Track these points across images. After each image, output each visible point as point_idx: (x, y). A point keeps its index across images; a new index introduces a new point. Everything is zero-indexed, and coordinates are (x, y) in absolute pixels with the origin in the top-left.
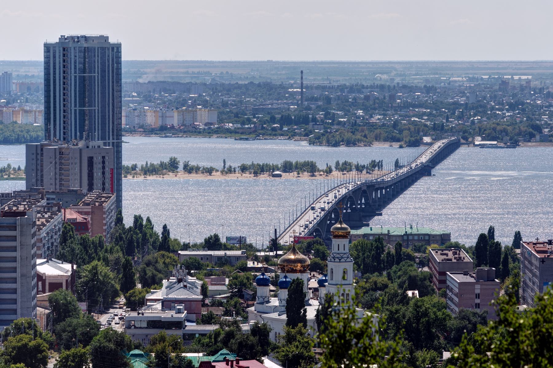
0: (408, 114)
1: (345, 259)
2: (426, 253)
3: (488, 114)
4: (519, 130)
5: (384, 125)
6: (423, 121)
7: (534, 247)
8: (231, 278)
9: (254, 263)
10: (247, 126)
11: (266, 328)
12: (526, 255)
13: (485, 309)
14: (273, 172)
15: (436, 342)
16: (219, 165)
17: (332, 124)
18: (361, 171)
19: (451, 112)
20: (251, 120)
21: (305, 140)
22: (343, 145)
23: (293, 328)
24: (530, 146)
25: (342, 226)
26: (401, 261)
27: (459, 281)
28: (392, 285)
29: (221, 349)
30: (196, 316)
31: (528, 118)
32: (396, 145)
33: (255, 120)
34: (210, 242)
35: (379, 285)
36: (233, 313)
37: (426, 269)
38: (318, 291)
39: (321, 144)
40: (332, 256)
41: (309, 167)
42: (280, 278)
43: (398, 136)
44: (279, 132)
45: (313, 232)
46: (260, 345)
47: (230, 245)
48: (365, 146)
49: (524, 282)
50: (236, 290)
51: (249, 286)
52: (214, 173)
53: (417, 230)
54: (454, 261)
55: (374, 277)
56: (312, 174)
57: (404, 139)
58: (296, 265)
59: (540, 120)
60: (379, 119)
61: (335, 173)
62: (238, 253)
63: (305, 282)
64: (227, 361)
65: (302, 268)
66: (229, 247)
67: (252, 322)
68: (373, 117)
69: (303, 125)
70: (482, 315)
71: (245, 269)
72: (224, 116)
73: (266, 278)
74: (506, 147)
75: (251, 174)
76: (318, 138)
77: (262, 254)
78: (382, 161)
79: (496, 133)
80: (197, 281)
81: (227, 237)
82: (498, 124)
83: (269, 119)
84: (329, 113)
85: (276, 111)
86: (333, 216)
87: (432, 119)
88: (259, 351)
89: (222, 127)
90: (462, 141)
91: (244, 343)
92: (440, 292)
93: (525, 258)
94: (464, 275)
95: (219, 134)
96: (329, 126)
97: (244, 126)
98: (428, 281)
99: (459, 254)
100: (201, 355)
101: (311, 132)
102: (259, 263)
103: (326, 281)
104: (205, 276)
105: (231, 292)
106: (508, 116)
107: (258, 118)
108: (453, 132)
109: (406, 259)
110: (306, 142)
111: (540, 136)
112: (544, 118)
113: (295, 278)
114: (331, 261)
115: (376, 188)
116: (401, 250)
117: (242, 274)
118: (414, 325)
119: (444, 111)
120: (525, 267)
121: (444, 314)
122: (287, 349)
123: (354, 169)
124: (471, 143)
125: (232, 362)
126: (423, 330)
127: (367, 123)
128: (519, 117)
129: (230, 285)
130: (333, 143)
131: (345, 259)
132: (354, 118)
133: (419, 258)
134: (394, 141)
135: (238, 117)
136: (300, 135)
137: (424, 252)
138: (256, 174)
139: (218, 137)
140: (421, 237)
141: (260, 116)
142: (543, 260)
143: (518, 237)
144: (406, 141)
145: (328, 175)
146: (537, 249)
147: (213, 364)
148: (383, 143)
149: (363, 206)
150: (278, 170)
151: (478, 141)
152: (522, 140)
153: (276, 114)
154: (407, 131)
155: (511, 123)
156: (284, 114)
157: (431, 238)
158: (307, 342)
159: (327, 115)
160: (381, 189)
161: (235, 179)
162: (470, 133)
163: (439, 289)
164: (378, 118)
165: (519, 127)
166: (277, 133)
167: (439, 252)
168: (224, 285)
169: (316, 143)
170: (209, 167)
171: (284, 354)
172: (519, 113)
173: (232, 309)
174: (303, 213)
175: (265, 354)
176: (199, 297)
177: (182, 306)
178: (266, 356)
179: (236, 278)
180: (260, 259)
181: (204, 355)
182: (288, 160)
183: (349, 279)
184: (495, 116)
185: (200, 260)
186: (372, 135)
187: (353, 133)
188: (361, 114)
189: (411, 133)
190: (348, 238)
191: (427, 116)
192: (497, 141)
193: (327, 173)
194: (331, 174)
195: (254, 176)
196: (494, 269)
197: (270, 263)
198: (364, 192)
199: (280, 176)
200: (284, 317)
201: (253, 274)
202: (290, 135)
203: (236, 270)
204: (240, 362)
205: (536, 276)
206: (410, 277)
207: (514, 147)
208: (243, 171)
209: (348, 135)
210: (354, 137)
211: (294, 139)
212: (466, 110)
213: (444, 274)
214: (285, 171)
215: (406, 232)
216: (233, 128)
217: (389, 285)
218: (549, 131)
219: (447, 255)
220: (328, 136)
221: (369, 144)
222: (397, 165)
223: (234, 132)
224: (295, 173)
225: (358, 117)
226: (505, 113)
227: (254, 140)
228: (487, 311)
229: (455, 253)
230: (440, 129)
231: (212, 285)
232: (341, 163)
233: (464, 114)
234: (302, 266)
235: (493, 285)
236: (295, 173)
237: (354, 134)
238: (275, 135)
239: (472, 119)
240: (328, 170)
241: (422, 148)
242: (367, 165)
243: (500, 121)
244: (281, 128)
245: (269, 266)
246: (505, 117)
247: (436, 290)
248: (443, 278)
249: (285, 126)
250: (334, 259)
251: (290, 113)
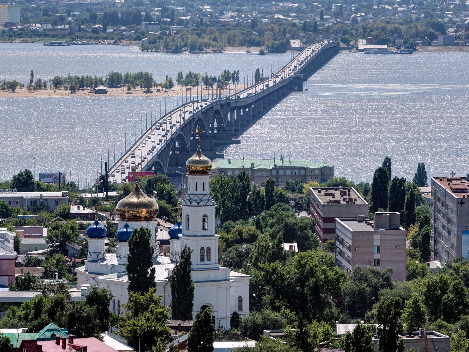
0: (270, 10)
1: (206, 202)
2: (302, 193)
3: (374, 9)
4: (416, 31)
5: (238, 25)
6: (290, 19)
7: (449, 184)
8: (50, 228)
9: (79, 207)
10: (59, 27)
11: (106, 295)
12: (439, 195)
13: (389, 267)
14: (96, 86)
15: (327, 310)
16: (24, 78)
17: (171, 23)
18: (211, 85)
19: (326, 6)
20: (65, 20)
21: (136, 45)
22: (186, 51)
23: (142, 294)
24: (430, 51)
25: (201, 158)
26: (273, 204)
27: (352, 231)
28: (262, 235)
29: (47, 324)
30: (9, 280)
31: (427, 14)
32: (255, 50)
33: (70, 19)
34: (21, 180)
35: (244, 236)
36: (55, 275)
37: (304, 214)
38: (169, 244)
39: (157, 50)
40: (188, 198)
41: (143, 80)
42: (119, 228)
43: (258, 38)
44: (102, 34)
45: (152, 165)
46: (98, 316)
47: (44, 184)
48: (215, 52)
49: (436, 230)
50: (57, 244)
51: (75, 238)
52: (18, 89)
53: (289, 163)
54: (343, 203)
55: (238, 226)
56: (146, 89)
57: (266, 43)
58: (140, 210)
59: (443, 17)
60: (232, 17)
61: (177, 88)
62: (58, 194)
63: (153, 233)
64: (58, 340)
65: (148, 215)
66: (44, 187)
67: (85, 286)
68: (223, 14)
69: (134, 25)
70: (384, 274)
71: (67, 216)
72: (29, 14)
73: (100, 229)
74: (399, 52)
75: (66, 90)
76: (154, 42)
77: (89, 195)
78: (238, 71)
79: (385, 34)
80: (8, 233)
81: (40, 174)
82: (388, 23)
83: (88, 18)
84: (167, 10)
85: (98, 6)
86: (177, 145)
87: (302, 16)
88: (97, 326)
89: (27, 28)
90: (342, 45)
91: (77, 315)
92: (325, 244)
93: (438, 199)
94: (359, 222)
95: (23, 37)
96: (167, 26)
97: (55, 27)
98: (309, 230)
99: (349, 195)
100: (20, 330)
101: (143, 35)
102: (86, 208)
103: (179, 231)
104: (16, 226)
105: (51, 247)
106: (401, 12)
107: (74, 16)
108: (330, 33)
109: (278, 201)
110: (137, 47)
111: (444, 38)
112: (448, 14)
113: (139, 228)
114: (186, 206)
115: (232, 107)
116: (273, 189)
117: (64, 222)
118: (297, 288)
119: (317, 6)
120: (437, 210)
121: (336, 273)
122: (135, 322)
123: (201, 82)
124: (353, 47)
125: (64, 340)
126: (310, 295)
127: (216, 22)
128: (416, 13)
129: (49, 238)
130: (174, 48)
131: (206, 202)
132: (199, 15)
133: (295, 200)
134: (253, 46)
135: (47, 15)
136: (129, 38)
137: (301, 191)
138: (73, 90)
139: (22, 42)
140: (294, 171)
141: (77, 13)
142: (461, 201)
143: (421, 170)
144: (268, 46)
145: (167, 90)
146: (454, 187)
147: (39, 343)
148: (238, 48)
149: (216, 132)
150: (102, 84)
151: (362, 44)
152: (420, 43)
153: (97, 11)
154: (269, 33)
155: (404, 21)
156: (107, 10)
157: (309, 174)
158: (162, 313)
159: (164, 11)
160: (239, 108)
161: (47, 96)
162: (352, 35)
163: (324, 241)
164: (231, 15)
165: (416, 26)
166: (99, 35)
167: (323, 192)
168: (41, 236)
169: (151, 49)
170: (12, 81)
171: (130, 328)
172: (414, 8)
173: (54, 269)
174: (138, 140)
175: (104, 329)
176: (12, 254)
178: (107, 332)
179: (57, 228)
180: (86, 202)
181: (24, 332)
182: (116, 71)
183: (209, 229)
184: (383, 12)
185: (8, 204)
186: (225, 37)
187: (199, 35)
188: (208, 10)
189: (274, 34)
190: (208, 174)
191: (296, 12)
192: (387, 44)
193: (167, 88)
194: (172, 89)
195: (71, 93)
196: (398, 213)
197: (100, 207)
198: (217, 112)
199: (105, 92)
200: (125, 279)
201: (78, 222)
202: (116, 38)
203: (55, 217)
204: (75, 340)
205: (453, 224)
206: (286, 224)
207: (410, 53)
208: (56, 87)
209: (192, 38)
210: (200, 40)
211: (122, 44)
212: (346, 4)
213: (332, 220)
214: (111, 86)
215: (275, 165)
216: (41, 30)
217: (259, 236)
218: (456, 32)
219: (333, 195)
220: (166, 40)
221: (219, 50)
222: (259, 78)
223: (42, 35)
224: (125, 88)
225: (205, 15)
226: (397, 8)
227: (70, 45)
228: (391, 270)
229: (343, 194)
230: (312, 29)
231: (25, 237)
232: (184, 76)
233: (344, 10)
234: (148, 212)
235: (396, 235)
236: (125, 88)
237: (200, 37)
238: (97, 38)
239: (353, 16)
240: (168, 84)
241: (289, 55)
242: (219, 77)
243: (390, 18)
244: (104, 30)
245: (99, 211)
246: (396, 14)
247: (320, 242)
248: (329, 226)
249: (110, 27)
250: (191, 203)
251: (116, 10)
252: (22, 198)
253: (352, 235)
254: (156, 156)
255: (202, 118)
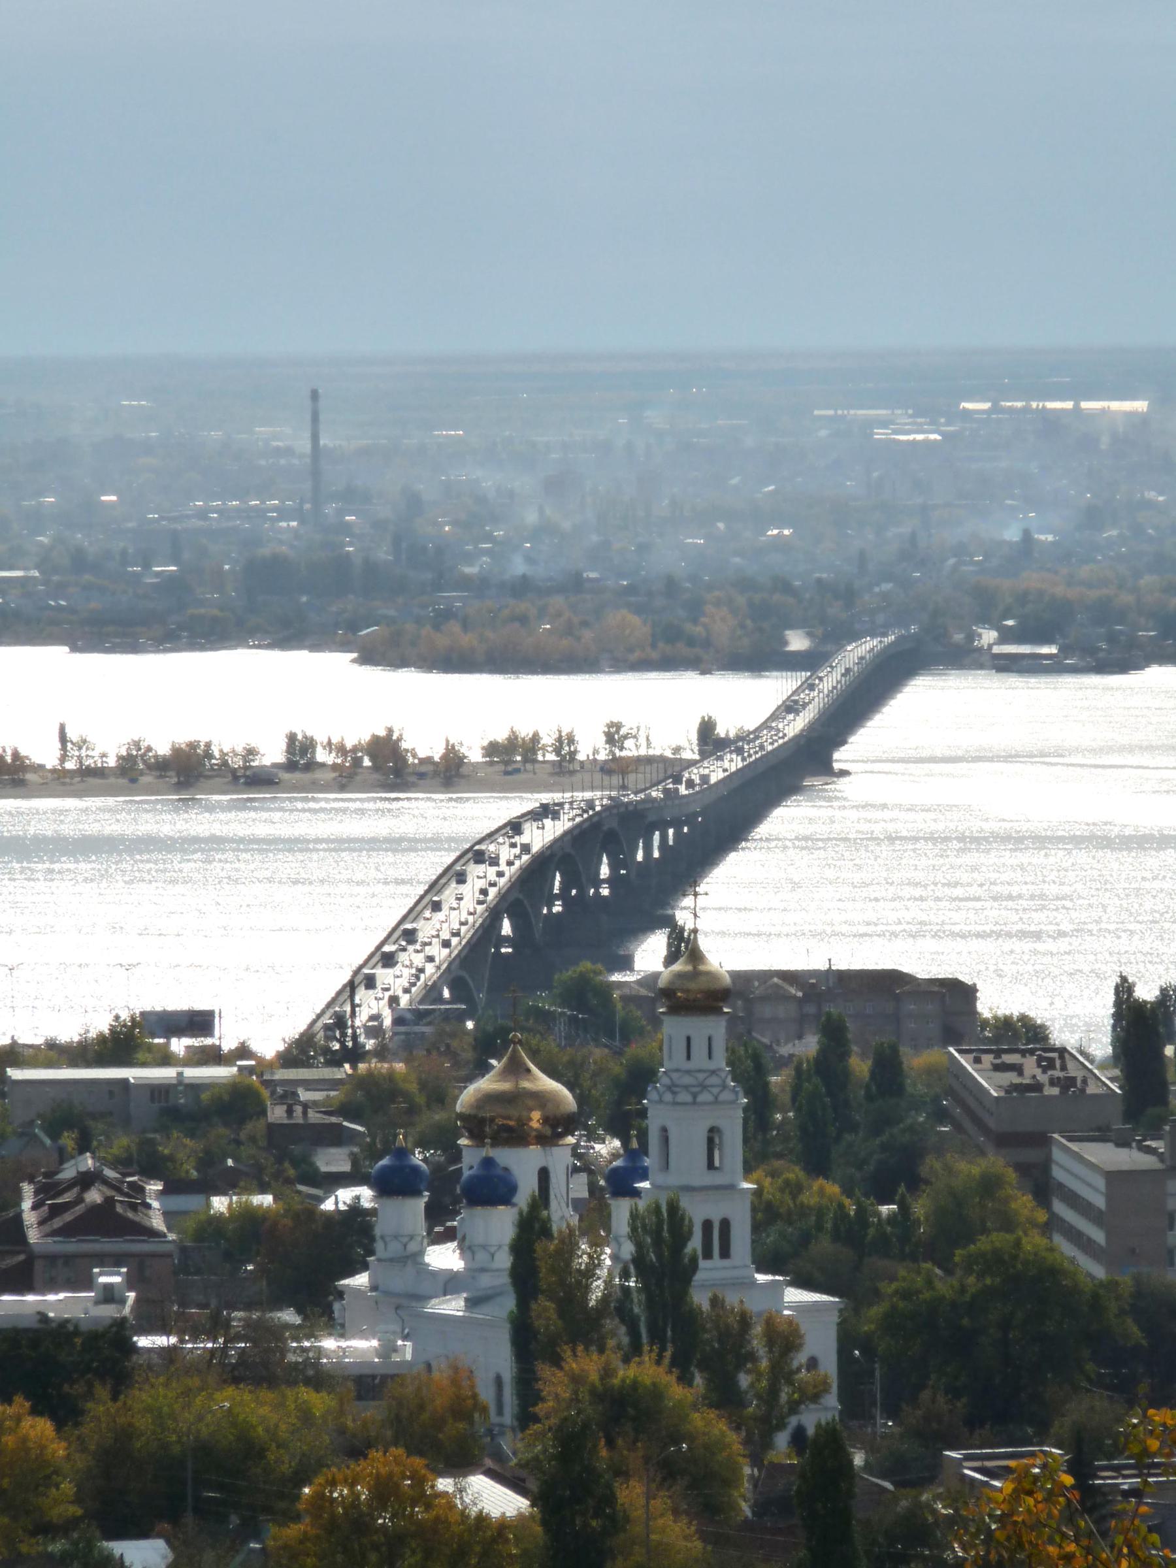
99: (1064, 1068)
167: (988, 1059)
177: (118, 1274)
219: (1018, 1069)
252: (124, 1082)
253: (1109, 1184)
254: (457, 961)
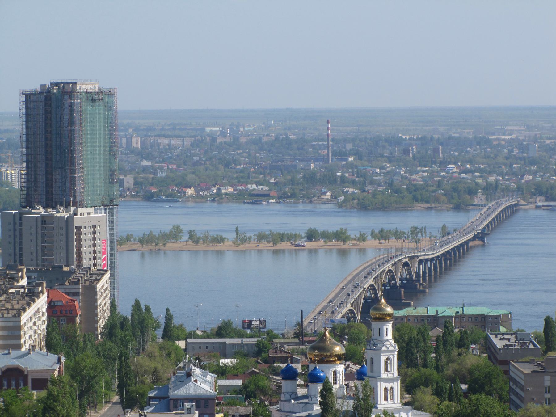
114: (371, 349)
255: (392, 269)
